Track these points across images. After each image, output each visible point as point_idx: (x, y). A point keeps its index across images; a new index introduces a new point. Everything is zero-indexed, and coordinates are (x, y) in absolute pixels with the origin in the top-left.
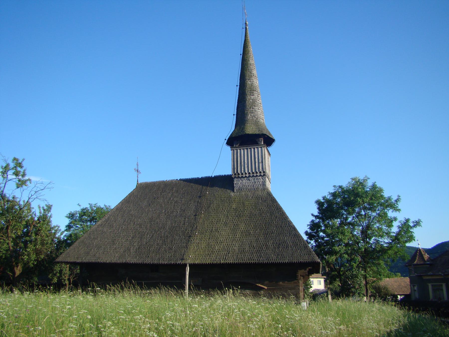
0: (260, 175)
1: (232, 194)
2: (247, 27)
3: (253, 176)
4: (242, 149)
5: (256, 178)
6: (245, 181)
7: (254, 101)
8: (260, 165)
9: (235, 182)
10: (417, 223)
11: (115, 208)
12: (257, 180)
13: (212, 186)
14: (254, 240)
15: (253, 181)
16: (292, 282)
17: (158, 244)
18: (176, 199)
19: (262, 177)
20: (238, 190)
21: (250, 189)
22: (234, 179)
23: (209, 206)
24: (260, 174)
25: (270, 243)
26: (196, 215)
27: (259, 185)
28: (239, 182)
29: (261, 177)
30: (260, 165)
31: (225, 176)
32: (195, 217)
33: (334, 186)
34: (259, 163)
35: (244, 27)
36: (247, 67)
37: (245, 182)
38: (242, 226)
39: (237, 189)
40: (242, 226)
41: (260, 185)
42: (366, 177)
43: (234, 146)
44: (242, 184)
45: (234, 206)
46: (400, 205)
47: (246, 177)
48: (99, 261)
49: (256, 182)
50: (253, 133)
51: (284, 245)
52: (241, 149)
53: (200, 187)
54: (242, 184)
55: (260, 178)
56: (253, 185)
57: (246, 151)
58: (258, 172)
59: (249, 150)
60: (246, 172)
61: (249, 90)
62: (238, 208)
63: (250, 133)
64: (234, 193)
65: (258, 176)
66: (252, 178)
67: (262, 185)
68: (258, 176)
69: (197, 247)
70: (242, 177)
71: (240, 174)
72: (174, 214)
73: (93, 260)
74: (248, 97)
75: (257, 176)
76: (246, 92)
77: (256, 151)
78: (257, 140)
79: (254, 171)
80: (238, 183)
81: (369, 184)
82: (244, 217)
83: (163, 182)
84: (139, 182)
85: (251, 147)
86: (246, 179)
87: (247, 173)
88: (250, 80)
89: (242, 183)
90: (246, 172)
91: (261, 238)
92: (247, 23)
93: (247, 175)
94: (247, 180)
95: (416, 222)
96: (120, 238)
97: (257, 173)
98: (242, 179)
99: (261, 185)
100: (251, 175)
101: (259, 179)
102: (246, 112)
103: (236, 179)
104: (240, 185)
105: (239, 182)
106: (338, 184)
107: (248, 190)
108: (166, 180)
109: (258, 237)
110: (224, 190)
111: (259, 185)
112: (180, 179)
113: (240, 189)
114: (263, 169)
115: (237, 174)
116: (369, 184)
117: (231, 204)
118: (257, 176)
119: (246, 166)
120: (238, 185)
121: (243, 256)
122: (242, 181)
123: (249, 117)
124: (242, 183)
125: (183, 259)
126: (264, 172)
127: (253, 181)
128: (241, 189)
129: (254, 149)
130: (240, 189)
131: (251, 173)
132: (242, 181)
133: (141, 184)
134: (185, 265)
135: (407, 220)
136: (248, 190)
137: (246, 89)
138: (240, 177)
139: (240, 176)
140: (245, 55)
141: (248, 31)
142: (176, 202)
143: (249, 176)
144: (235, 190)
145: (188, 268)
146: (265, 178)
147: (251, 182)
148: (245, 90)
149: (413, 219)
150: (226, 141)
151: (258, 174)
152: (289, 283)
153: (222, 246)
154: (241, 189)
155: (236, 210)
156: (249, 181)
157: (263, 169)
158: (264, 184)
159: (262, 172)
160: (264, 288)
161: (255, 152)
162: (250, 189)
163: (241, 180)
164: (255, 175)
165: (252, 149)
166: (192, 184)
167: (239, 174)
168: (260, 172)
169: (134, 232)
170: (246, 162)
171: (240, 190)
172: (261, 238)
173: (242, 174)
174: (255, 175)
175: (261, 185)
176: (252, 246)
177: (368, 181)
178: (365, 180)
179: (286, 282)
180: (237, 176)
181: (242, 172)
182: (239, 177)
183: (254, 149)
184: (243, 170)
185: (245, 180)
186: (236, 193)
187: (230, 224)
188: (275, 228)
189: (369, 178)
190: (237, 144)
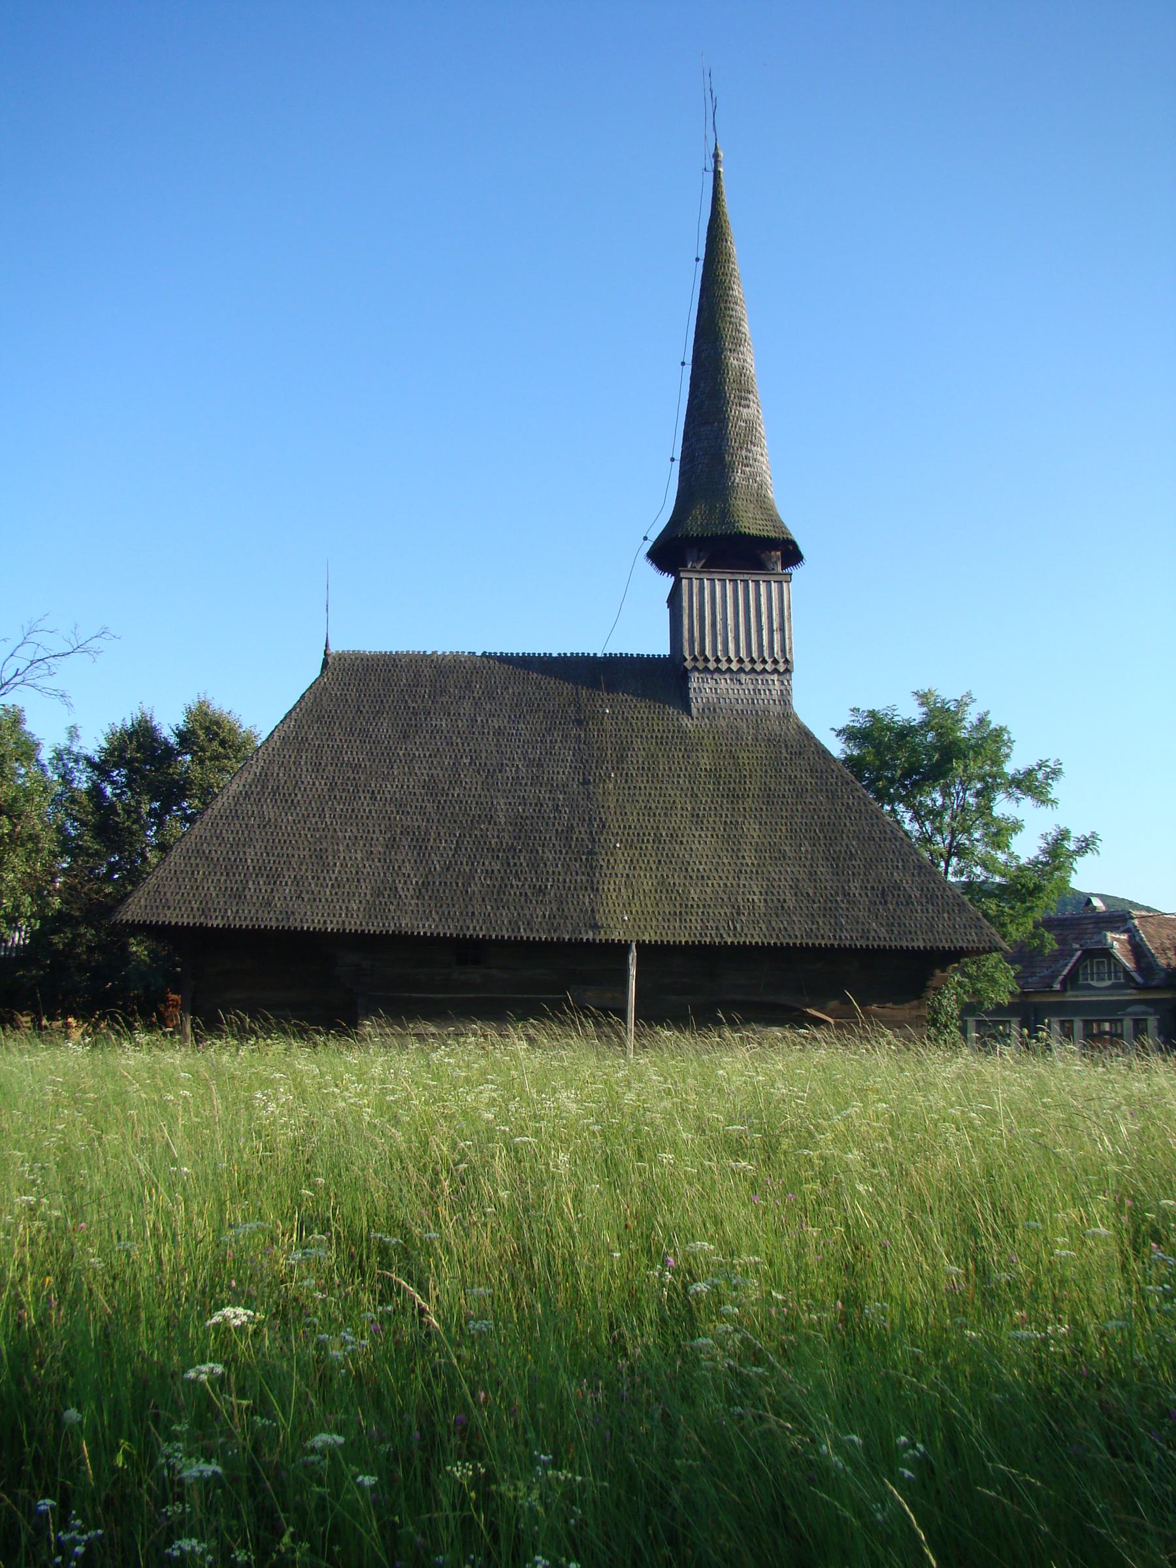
0: (776, 671)
1: (686, 721)
2: (721, 170)
3: (753, 670)
4: (719, 580)
5: (761, 677)
6: (724, 684)
7: (751, 428)
8: (777, 637)
9: (693, 684)
10: (1087, 845)
11: (276, 734)
12: (763, 684)
13: (611, 688)
14: (804, 877)
15: (751, 687)
16: (907, 1005)
17: (490, 873)
18: (495, 723)
19: (781, 678)
20: (703, 710)
21: (742, 711)
22: (690, 675)
23: (622, 755)
24: (773, 667)
25: (855, 887)
26: (586, 782)
27: (771, 702)
28: (706, 685)
29: (775, 677)
30: (777, 637)
31: (640, 658)
32: (587, 790)
33: (855, 710)
34: (771, 631)
35: (711, 167)
36: (725, 308)
37: (727, 686)
38: (752, 829)
39: (701, 705)
40: (752, 829)
41: (774, 701)
42: (968, 695)
43: (689, 566)
44: (716, 692)
45: (705, 762)
46: (1056, 790)
47: (729, 670)
48: (295, 923)
49: (762, 692)
50: (762, 533)
51: (899, 895)
52: (736, 580)
53: (568, 688)
54: (716, 692)
55: (773, 681)
56: (753, 700)
57: (729, 587)
58: (767, 658)
59: (695, 583)
60: (732, 655)
61: (735, 386)
62: (721, 770)
63: (754, 532)
64: (692, 719)
65: (768, 673)
66: (748, 677)
67: (779, 701)
68: (768, 673)
69: (630, 890)
70: (718, 670)
71: (712, 659)
72: (510, 772)
73: (270, 920)
74: (734, 411)
75: (764, 671)
76: (725, 393)
77: (762, 589)
78: (763, 556)
79: (755, 655)
80: (702, 689)
81: (971, 717)
82: (750, 800)
83: (424, 657)
84: (333, 649)
85: (746, 577)
86: (727, 676)
87: (732, 657)
88: (736, 355)
89: (716, 689)
90: (732, 655)
91: (822, 869)
92: (721, 154)
93: (734, 666)
94: (731, 680)
95: (1086, 840)
96: (341, 845)
97: (764, 662)
98: (716, 676)
99: (777, 702)
100: (748, 667)
101: (770, 682)
102: (728, 458)
103: (697, 674)
104: (710, 695)
105: (706, 685)
106: (866, 707)
107: (734, 712)
108: (434, 653)
109: (453, 856)
110: (655, 706)
111: (771, 702)
112: (485, 652)
113: (709, 709)
114: (783, 650)
115: (701, 659)
116: (971, 717)
117: (694, 754)
118: (764, 671)
119: (730, 638)
120: (702, 695)
121: (785, 923)
122: (717, 683)
123: (738, 477)
124: (716, 689)
125: (595, 927)
126: (787, 661)
127: (751, 687)
128: (714, 709)
129: (757, 583)
130: (709, 709)
131: (746, 660)
132: (717, 683)
133: (341, 657)
134: (624, 948)
135: (1064, 835)
136: (734, 712)
137: (725, 382)
138: (712, 669)
139: (712, 665)
140: (717, 266)
141: (724, 184)
142: (499, 732)
143: (741, 670)
144: (694, 711)
145: (1128, 960)
146: (788, 681)
147: (744, 687)
148: (722, 383)
149: (1078, 831)
150: (648, 545)
151: (769, 667)
152: (896, 1007)
153: (709, 891)
154: (714, 709)
155: (714, 774)
156: (738, 686)
157: (783, 650)
158: (785, 699)
159: (781, 661)
160: (827, 1021)
161: (760, 595)
162: (742, 711)
163: (712, 678)
164: (759, 667)
165: (751, 584)
166: (535, 675)
167: (706, 660)
168: (775, 662)
169: (383, 826)
170: (729, 622)
171: (711, 710)
172: (822, 869)
173: (718, 660)
174: (759, 667)
175: (777, 702)
176: (802, 895)
177: (969, 709)
178: (961, 704)
179: (888, 1005)
180: (700, 665)
181: (719, 654)
182: (706, 670)
183: (757, 583)
184: (720, 647)
185: (726, 679)
186: (697, 718)
187: (711, 820)
188: (854, 843)
189: (974, 701)
190: (699, 560)
